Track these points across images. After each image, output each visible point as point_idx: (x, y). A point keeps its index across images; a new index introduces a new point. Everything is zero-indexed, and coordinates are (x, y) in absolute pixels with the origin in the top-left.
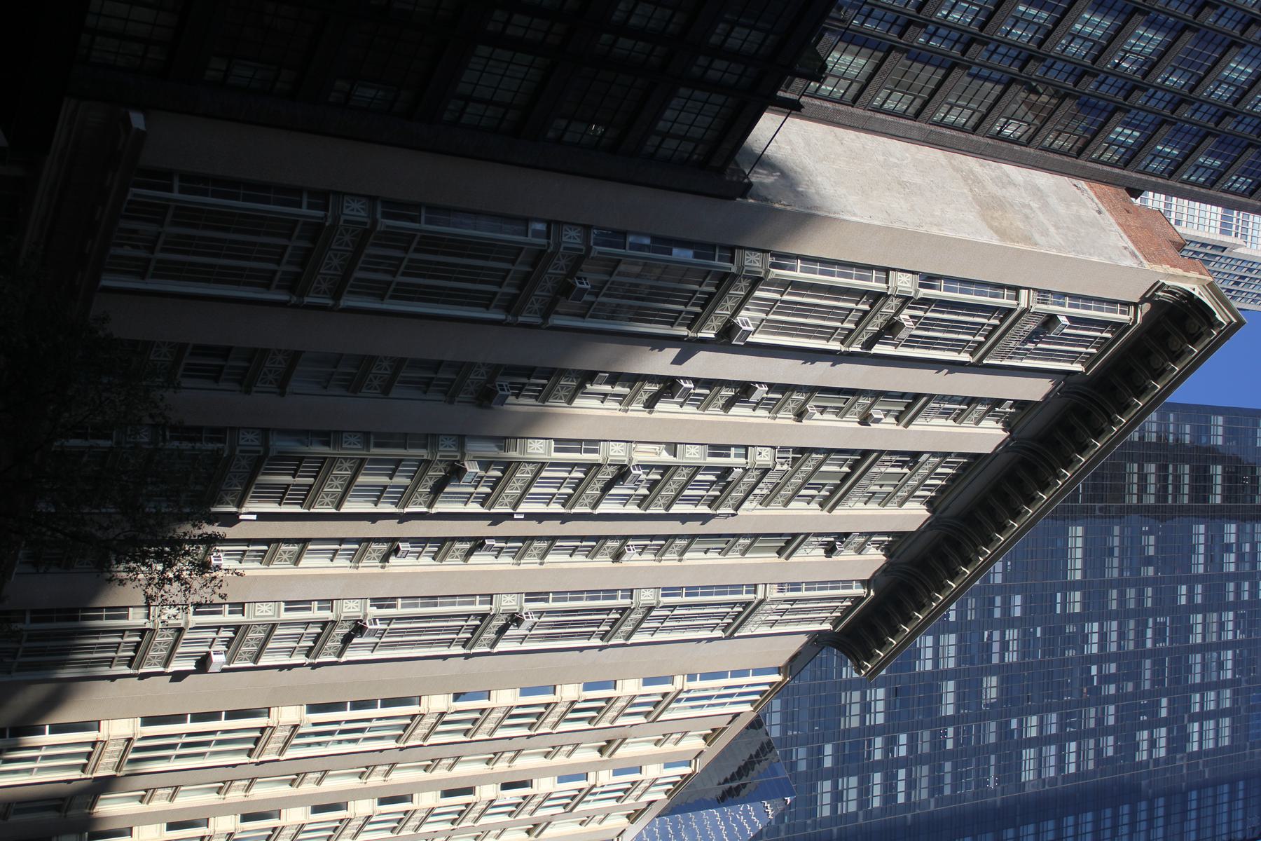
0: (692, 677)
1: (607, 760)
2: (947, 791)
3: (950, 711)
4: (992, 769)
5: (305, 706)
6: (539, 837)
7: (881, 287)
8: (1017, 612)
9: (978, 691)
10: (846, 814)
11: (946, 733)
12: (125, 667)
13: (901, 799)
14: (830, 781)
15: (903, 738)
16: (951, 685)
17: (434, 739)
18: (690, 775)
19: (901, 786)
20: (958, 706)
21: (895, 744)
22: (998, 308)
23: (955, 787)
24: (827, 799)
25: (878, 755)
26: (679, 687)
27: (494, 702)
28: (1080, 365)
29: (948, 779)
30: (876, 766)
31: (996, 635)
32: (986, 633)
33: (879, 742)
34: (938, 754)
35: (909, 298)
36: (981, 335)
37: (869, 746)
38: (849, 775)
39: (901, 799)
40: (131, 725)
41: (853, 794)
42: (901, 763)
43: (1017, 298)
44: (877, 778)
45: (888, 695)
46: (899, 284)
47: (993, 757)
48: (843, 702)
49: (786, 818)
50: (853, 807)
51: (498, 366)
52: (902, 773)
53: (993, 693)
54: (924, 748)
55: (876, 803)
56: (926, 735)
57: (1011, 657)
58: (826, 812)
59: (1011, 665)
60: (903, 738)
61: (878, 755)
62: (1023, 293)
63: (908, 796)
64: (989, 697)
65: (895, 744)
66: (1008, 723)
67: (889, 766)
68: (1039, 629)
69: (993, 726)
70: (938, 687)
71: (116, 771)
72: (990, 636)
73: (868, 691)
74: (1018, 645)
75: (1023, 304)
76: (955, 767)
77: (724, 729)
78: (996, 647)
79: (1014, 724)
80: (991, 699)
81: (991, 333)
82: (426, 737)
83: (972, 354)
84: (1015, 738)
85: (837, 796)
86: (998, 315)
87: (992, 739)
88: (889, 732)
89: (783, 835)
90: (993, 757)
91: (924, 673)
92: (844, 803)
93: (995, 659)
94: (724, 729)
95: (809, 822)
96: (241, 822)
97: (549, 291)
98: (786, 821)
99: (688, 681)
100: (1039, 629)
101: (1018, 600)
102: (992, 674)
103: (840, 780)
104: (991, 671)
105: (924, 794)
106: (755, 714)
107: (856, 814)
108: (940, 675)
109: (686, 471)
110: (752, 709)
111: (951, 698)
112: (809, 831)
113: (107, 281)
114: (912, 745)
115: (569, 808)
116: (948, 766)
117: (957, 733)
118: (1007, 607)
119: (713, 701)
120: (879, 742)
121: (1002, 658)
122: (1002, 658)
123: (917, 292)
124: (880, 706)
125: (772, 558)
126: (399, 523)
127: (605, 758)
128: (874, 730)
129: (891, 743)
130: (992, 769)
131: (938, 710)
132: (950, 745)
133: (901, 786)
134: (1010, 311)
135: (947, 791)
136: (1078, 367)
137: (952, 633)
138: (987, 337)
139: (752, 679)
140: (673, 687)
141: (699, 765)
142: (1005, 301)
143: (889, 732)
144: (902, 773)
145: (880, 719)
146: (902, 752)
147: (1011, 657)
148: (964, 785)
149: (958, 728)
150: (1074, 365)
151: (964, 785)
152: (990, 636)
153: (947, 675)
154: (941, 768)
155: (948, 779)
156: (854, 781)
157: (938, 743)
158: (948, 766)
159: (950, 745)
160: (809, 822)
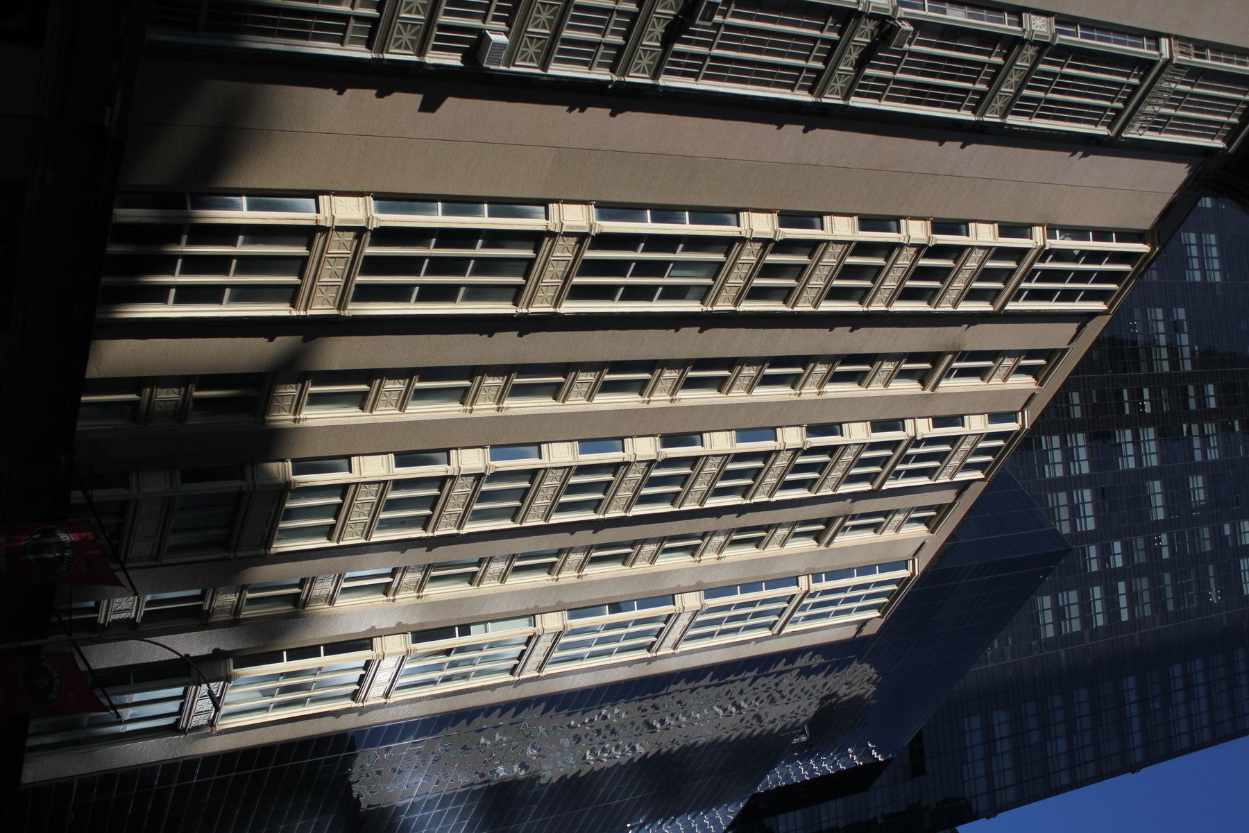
0: (817, 578)
1: (824, 551)
2: (1170, 606)
3: (1160, 515)
4: (1212, 580)
5: (410, 635)
6: (832, 546)
7: (1015, 30)
8: (1212, 403)
9: (1187, 492)
10: (1070, 634)
11: (1160, 540)
12: (363, 48)
13: (1125, 616)
14: (1049, 597)
15: (1117, 546)
16: (1157, 486)
17: (549, 670)
18: (909, 579)
19: (1123, 602)
20: (1168, 508)
21: (1111, 554)
22: (1139, 60)
23: (1178, 602)
24: (1049, 617)
25: (1094, 566)
26: (805, 588)
27: (709, 448)
28: (1220, 141)
29: (1169, 592)
30: (1093, 579)
31: (1195, 429)
32: (1185, 426)
33: (1093, 551)
34: (1154, 566)
35: (1045, 45)
36: (1119, 101)
37: (1084, 556)
38: (1068, 590)
39: (1125, 616)
40: (362, 208)
41: (1075, 611)
42: (1117, 574)
43: (1158, 48)
44: (1097, 592)
45: (1094, 495)
46: (1033, 28)
47: (1211, 568)
48: (1050, 505)
49: (1010, 639)
50: (1076, 626)
51: (429, 565)
52: (1122, 587)
53: (1201, 495)
54: (1140, 557)
55: (1100, 621)
56: (1140, 543)
57: (1213, 455)
58: (1050, 632)
59: (1214, 462)
60: (1117, 546)
61: (1094, 566)
62: (1164, 42)
63: (1131, 613)
64: (1197, 499)
65: (1111, 554)
66: (1221, 529)
67: (1108, 578)
68: (1236, 423)
69: (1206, 532)
70: (1145, 489)
71: (339, 309)
72: (1189, 431)
73: (1075, 492)
74: (1217, 441)
75: (1166, 55)
76: (1174, 579)
77: (951, 505)
78: (1197, 443)
79: (1227, 530)
80: (1200, 501)
81: (1131, 96)
82: (540, 668)
83: (1110, 126)
84: (1230, 545)
85: (1060, 614)
86: (1139, 71)
87: (1207, 546)
88: (1102, 537)
89: (1009, 660)
90: (1211, 568)
91: (1128, 472)
92: (1068, 622)
93: (1198, 456)
94: (951, 505)
95: (1034, 643)
96: (413, 643)
97: (657, 40)
98: (1010, 643)
99: (813, 583)
100: (1236, 423)
101: (1211, 389)
102: (1197, 474)
103: (1060, 595)
104: (1196, 469)
105: (1148, 611)
106: (883, 620)
107: (1080, 634)
108: (1147, 474)
109: (719, 460)
110: (880, 615)
111: (1159, 501)
112: (1036, 654)
113: (31, 742)
114: (1127, 554)
115: (776, 630)
116: (1167, 578)
117: (1170, 540)
118: (1202, 398)
119: (840, 607)
120: (1093, 551)
121: (1205, 455)
122: (1205, 455)
123: (1054, 37)
124: (1089, 509)
125: (809, 544)
126: (427, 551)
127: (928, 391)
128: (1087, 537)
129: (1106, 553)
130: (1212, 580)
131: (1148, 515)
132: (1166, 554)
133: (1123, 602)
134: (1152, 63)
135: (1170, 606)
136: (1218, 144)
137: (1150, 426)
138: (1126, 103)
139: (879, 577)
140: (799, 588)
141: (920, 565)
142: (1145, 51)
143: (1102, 537)
144: (1122, 587)
145: (1091, 525)
146: (1119, 562)
147: (1213, 455)
148: (1186, 599)
149: (1172, 534)
150: (1215, 141)
151: (1186, 599)
152: (1189, 431)
153: (1151, 474)
154: (1160, 580)
155: (1169, 592)
156: (1073, 596)
157: (1154, 552)
158: (1167, 578)
159: (1166, 554)
160: (1034, 643)
